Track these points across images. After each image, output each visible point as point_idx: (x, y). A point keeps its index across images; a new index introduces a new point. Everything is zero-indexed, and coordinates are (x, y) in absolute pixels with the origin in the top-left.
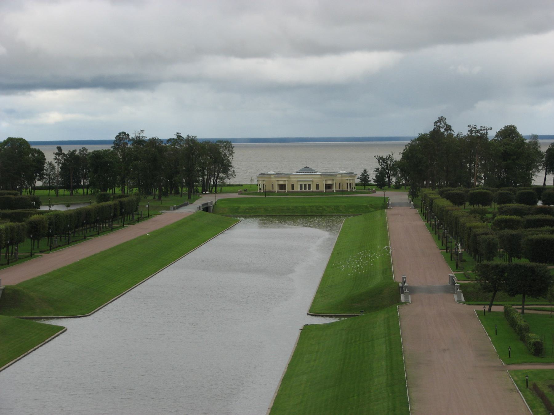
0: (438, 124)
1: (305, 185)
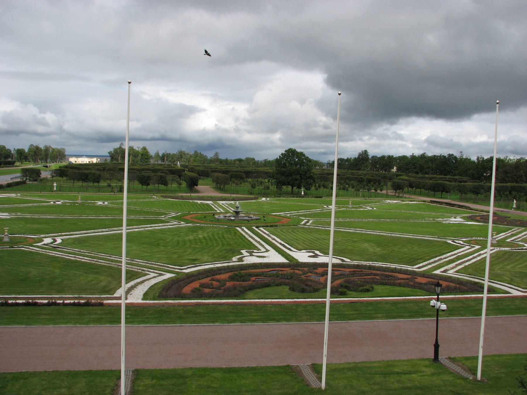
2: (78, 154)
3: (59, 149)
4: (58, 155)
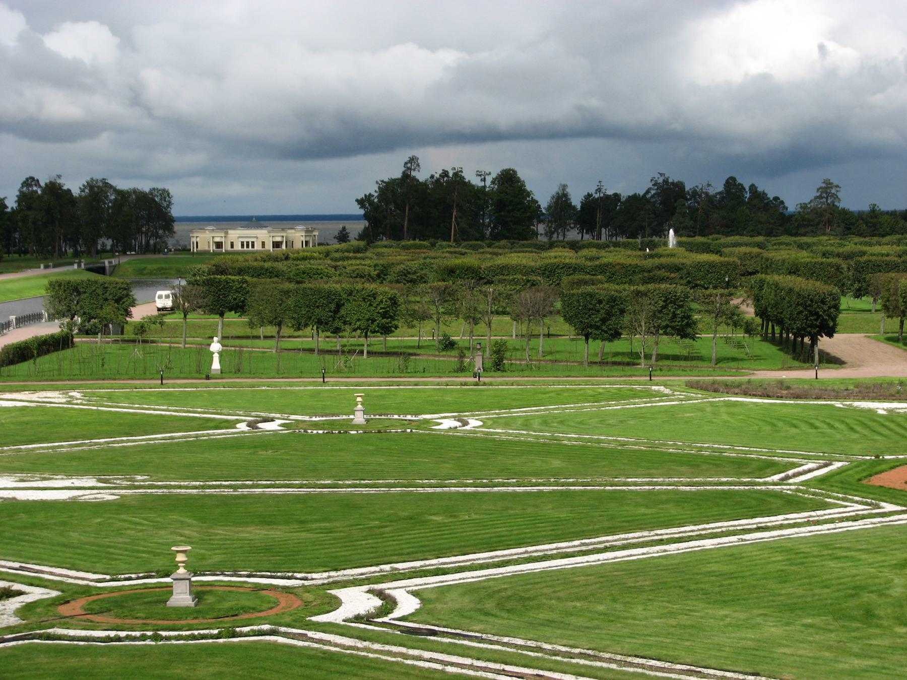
0: (409, 165)
1: (248, 243)
2: (295, 213)
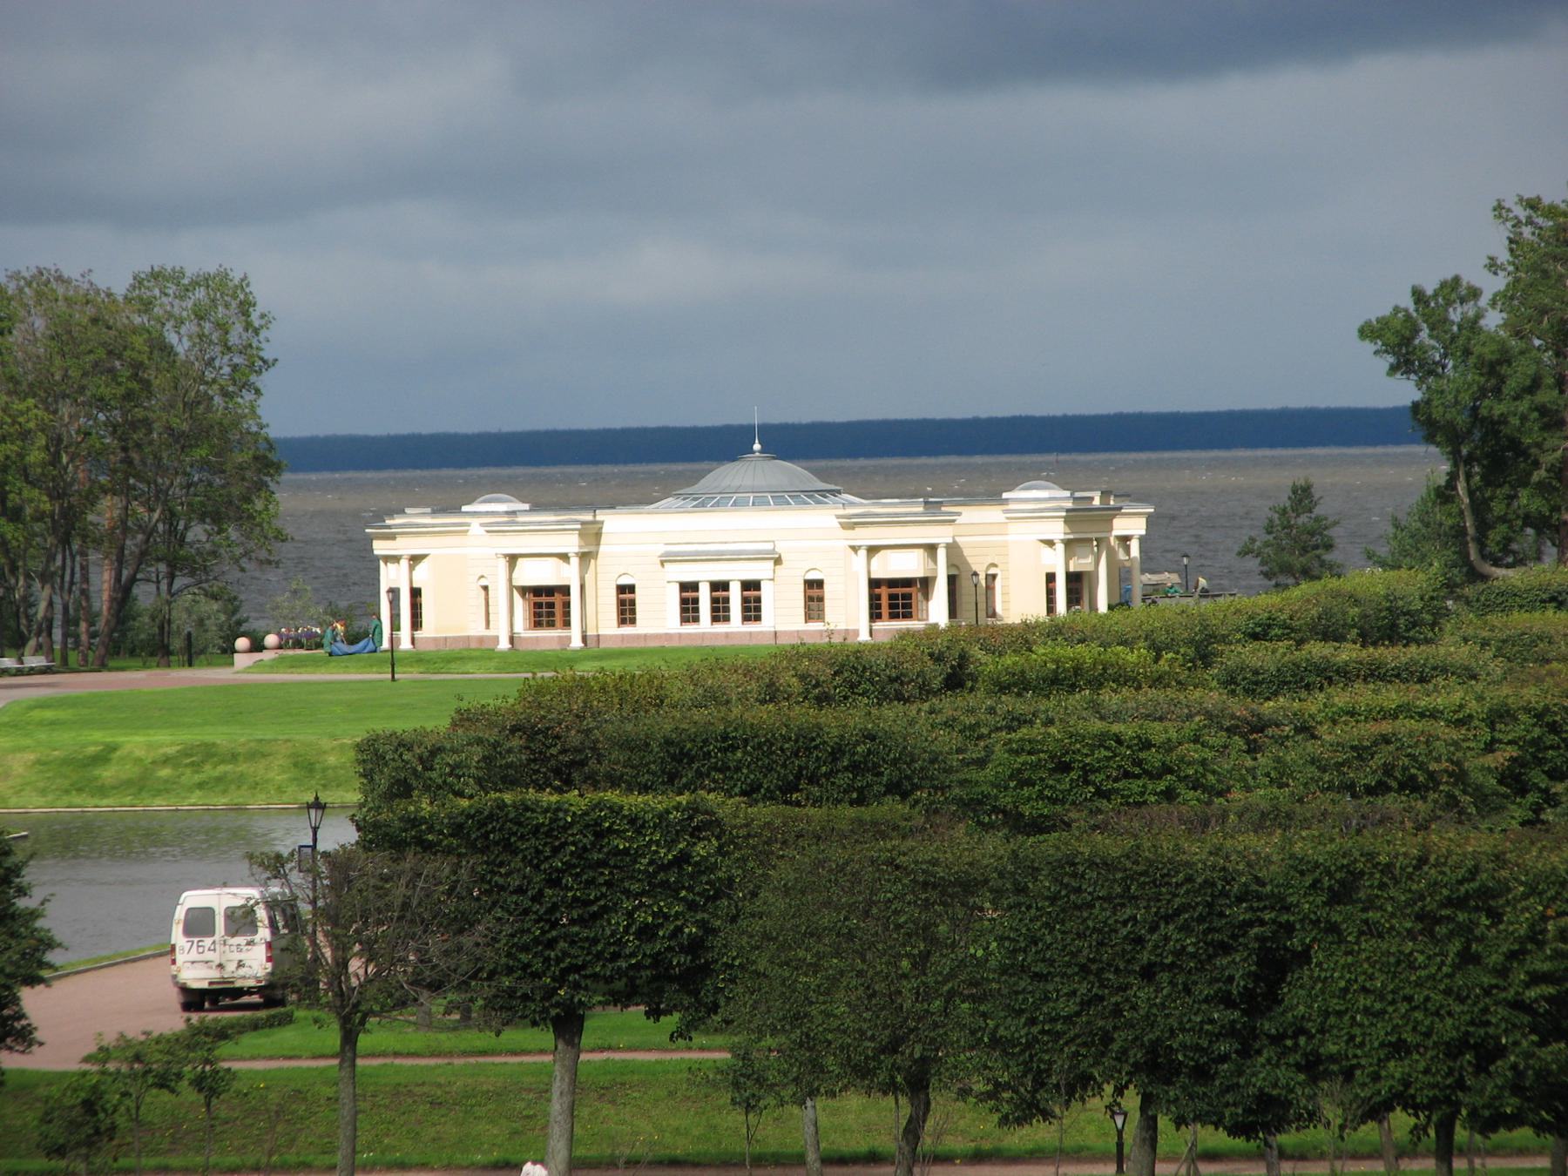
1: (720, 586)
3: (100, 311)
4: (78, 473)
